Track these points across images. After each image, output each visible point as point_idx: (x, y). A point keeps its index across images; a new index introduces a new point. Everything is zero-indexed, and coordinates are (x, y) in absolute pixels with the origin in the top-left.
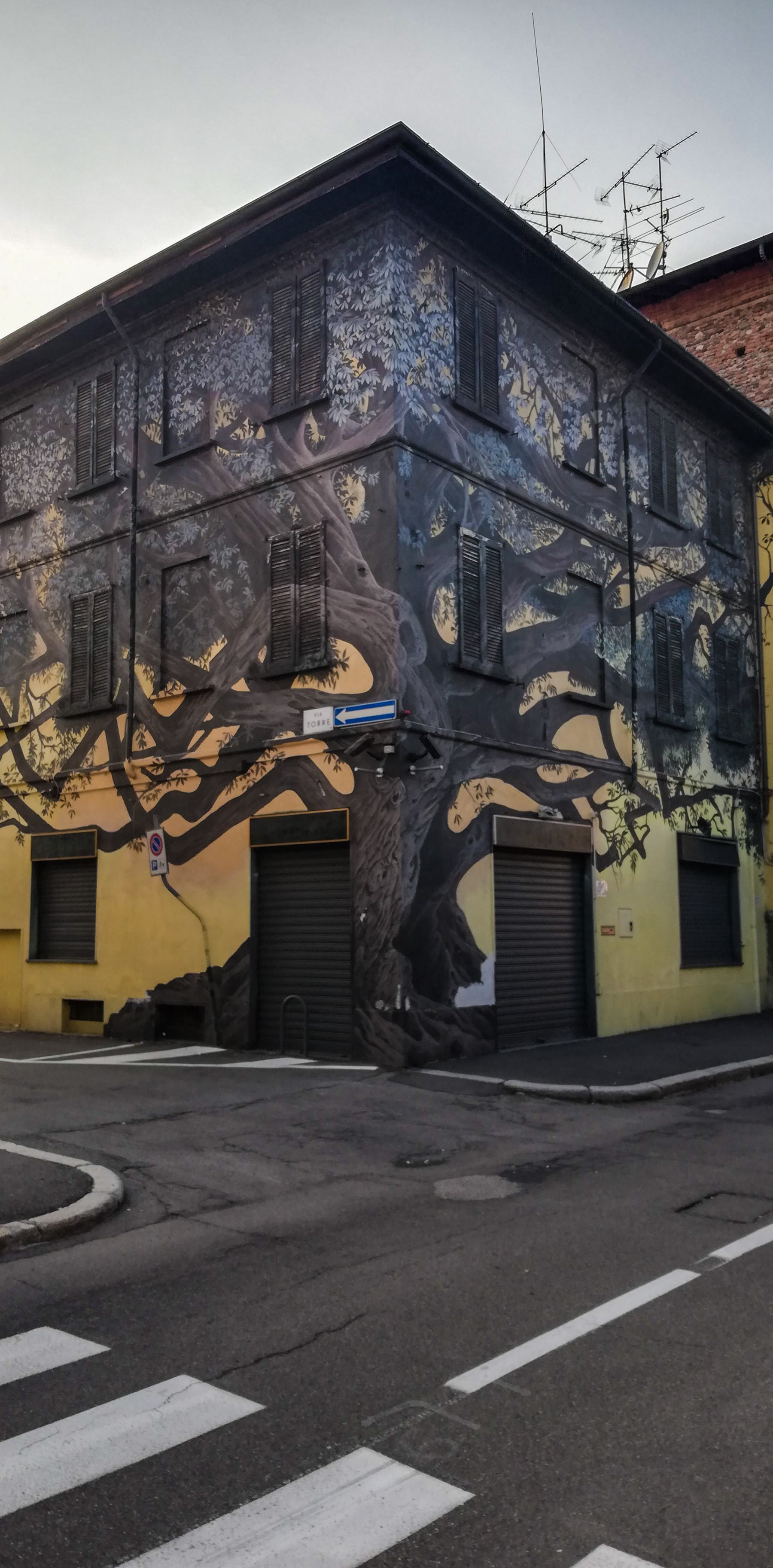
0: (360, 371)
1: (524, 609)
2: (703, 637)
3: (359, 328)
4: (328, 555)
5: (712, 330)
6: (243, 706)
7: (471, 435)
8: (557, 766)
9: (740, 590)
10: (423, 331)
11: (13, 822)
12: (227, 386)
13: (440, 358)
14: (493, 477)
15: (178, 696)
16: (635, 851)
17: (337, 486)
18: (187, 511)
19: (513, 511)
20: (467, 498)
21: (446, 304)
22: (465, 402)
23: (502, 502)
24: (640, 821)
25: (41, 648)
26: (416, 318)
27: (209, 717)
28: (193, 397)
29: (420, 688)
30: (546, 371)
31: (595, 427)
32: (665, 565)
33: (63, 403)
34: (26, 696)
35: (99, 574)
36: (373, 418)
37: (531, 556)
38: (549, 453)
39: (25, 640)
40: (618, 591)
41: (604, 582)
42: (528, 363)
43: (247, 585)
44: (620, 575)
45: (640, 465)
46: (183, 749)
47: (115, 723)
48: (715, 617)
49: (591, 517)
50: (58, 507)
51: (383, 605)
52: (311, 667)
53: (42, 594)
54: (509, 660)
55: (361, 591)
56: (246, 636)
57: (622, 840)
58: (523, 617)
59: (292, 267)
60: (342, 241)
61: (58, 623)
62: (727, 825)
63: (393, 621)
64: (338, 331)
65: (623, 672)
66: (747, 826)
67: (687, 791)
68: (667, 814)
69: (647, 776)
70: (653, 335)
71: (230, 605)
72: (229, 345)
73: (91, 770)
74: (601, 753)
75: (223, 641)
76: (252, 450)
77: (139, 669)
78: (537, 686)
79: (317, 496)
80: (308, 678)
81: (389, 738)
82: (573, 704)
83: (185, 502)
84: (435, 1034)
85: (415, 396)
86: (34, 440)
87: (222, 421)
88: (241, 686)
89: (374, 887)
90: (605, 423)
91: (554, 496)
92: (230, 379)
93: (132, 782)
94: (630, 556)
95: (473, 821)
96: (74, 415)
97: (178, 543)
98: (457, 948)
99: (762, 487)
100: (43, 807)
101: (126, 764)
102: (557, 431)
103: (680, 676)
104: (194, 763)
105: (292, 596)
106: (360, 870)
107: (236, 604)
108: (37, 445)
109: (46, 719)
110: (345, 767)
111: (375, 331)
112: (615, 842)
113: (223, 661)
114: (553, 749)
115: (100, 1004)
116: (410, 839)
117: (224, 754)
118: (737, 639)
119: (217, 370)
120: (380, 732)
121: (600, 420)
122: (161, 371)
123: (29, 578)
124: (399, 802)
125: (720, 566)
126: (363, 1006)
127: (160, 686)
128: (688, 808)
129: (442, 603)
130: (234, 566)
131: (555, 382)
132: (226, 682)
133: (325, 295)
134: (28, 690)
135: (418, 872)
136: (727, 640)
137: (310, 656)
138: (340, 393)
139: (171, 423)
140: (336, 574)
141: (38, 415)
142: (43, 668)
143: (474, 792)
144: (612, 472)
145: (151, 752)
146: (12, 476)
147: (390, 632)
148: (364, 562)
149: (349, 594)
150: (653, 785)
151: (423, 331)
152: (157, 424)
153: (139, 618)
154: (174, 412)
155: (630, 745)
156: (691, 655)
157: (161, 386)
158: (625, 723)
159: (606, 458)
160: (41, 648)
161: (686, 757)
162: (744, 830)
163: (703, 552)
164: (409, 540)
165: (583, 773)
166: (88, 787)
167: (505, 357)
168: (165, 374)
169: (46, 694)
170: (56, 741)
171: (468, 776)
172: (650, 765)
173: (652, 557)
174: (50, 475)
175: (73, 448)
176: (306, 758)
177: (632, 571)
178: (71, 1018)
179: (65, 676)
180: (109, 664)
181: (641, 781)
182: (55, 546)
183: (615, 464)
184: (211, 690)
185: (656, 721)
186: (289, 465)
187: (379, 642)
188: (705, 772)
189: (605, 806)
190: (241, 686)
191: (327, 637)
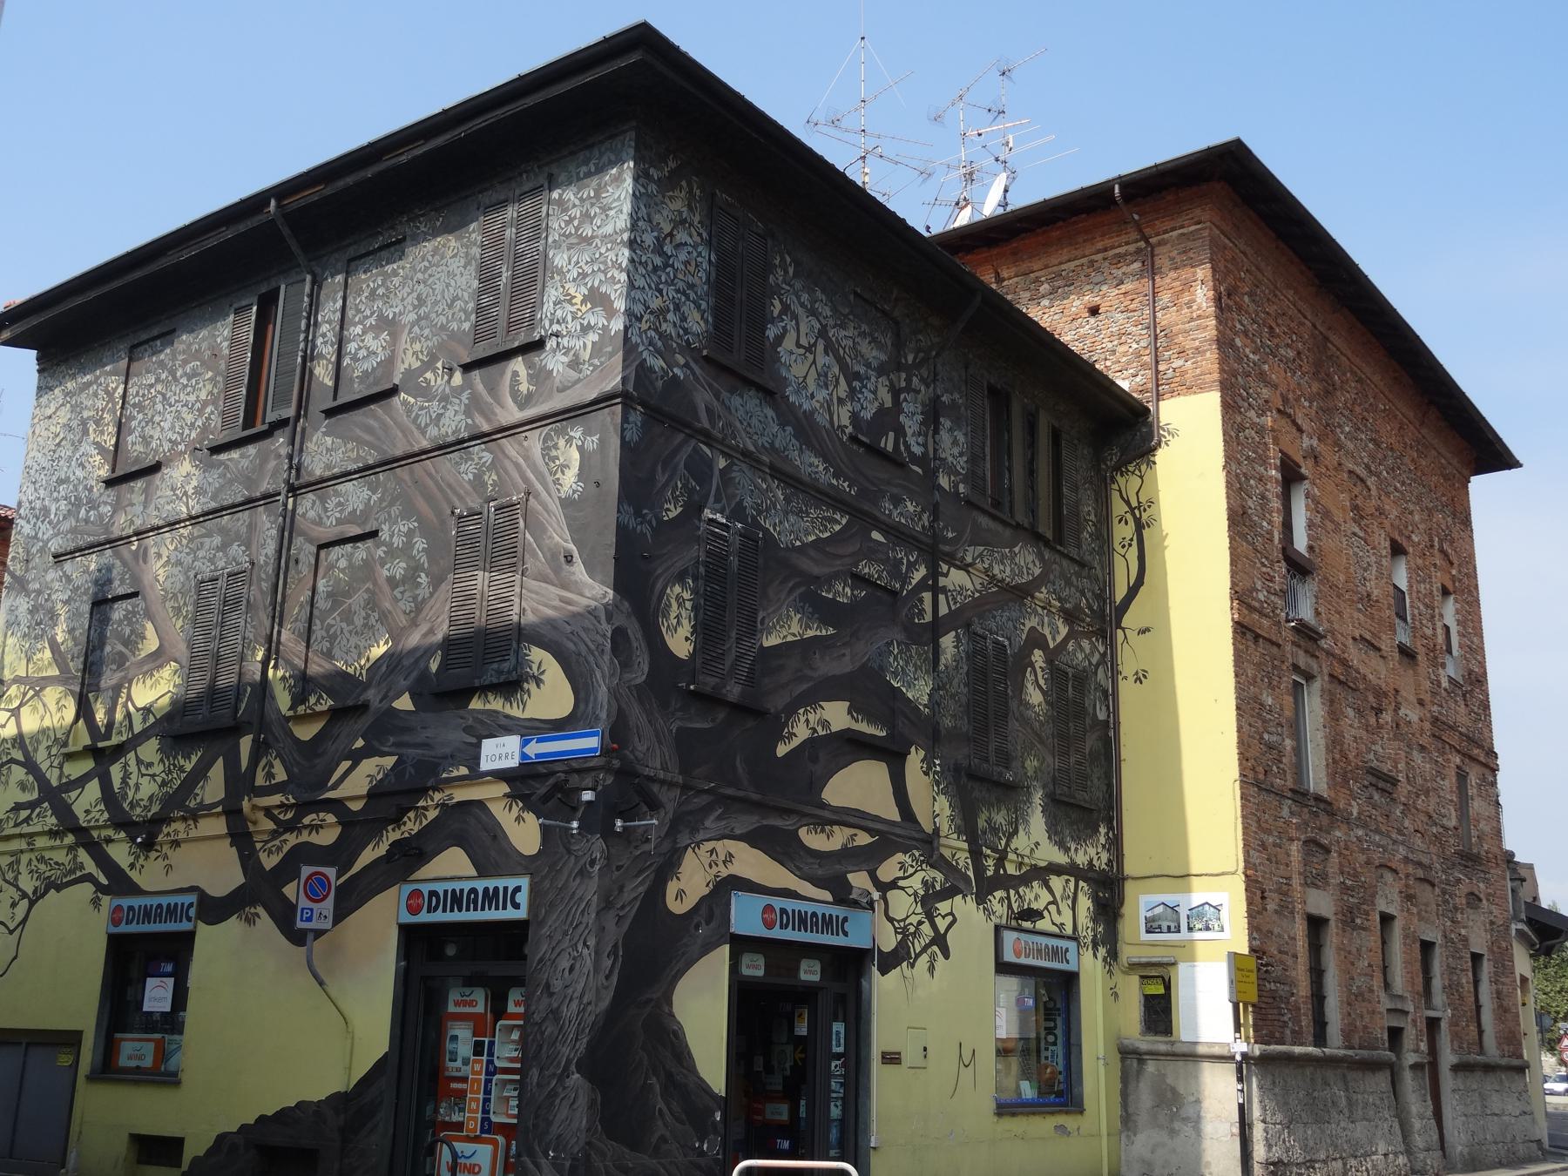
0: (584, 309)
1: (789, 617)
2: (1037, 666)
5: (1060, 283)
8: (827, 828)
9: (1090, 607)
10: (666, 265)
11: (89, 878)
12: (420, 318)
13: (688, 298)
14: (752, 448)
15: (322, 713)
16: (935, 948)
17: (546, 450)
18: (356, 472)
20: (717, 473)
21: (700, 235)
24: (944, 907)
25: (151, 643)
26: (659, 249)
27: (360, 743)
28: (377, 329)
29: (636, 714)
30: (831, 322)
31: (895, 392)
32: (986, 570)
35: (236, 550)
40: (921, 600)
41: (902, 587)
42: (808, 310)
43: (423, 570)
44: (924, 579)
45: (955, 443)
46: (322, 785)
48: (1054, 639)
49: (887, 505)
50: (193, 458)
52: (495, 681)
58: (787, 628)
61: (177, 611)
62: (1066, 917)
64: (560, 259)
65: (925, 706)
66: (1095, 920)
67: (1011, 869)
68: (981, 899)
69: (955, 847)
71: (399, 596)
72: (426, 268)
73: (199, 809)
74: (894, 814)
75: (386, 643)
76: (445, 399)
78: (803, 719)
79: (521, 461)
80: (491, 697)
81: (589, 781)
82: (852, 747)
83: (355, 461)
86: (172, 373)
87: (409, 360)
88: (404, 703)
89: (557, 985)
90: (908, 389)
91: (836, 476)
93: (252, 828)
94: (935, 554)
95: (703, 899)
96: (226, 344)
97: (341, 512)
98: (669, 1075)
99: (1118, 477)
100: (131, 859)
102: (843, 395)
103: (1004, 716)
104: (336, 806)
106: (541, 960)
107: (407, 594)
108: (175, 379)
109: (149, 738)
110: (530, 817)
111: (605, 263)
112: (906, 935)
113: (384, 668)
114: (824, 806)
115: (179, 1142)
116: (610, 921)
117: (374, 795)
118: (1084, 670)
120: (578, 771)
123: (146, 550)
124: (597, 867)
125: (1063, 575)
126: (532, 1155)
128: (1012, 892)
129: (675, 605)
130: (409, 545)
131: (843, 336)
134: (129, 698)
136: (1070, 670)
137: (495, 666)
139: (346, 361)
140: (537, 561)
143: (706, 859)
146: (140, 416)
147: (600, 640)
148: (572, 546)
150: (963, 859)
151: (666, 265)
152: (329, 361)
154: (351, 347)
155: (934, 807)
156: (1021, 687)
157: (338, 315)
158: (926, 773)
159: (909, 432)
160: (151, 643)
162: (1091, 925)
165: (864, 839)
166: (193, 833)
167: (777, 303)
171: (700, 837)
172: (959, 832)
173: (969, 559)
174: (189, 418)
176: (480, 804)
178: (139, 1162)
179: (178, 681)
182: (184, 509)
183: (920, 440)
184: (364, 708)
186: (489, 420)
187: (584, 650)
188: (1037, 844)
189: (894, 885)
190: (404, 703)
191: (519, 643)
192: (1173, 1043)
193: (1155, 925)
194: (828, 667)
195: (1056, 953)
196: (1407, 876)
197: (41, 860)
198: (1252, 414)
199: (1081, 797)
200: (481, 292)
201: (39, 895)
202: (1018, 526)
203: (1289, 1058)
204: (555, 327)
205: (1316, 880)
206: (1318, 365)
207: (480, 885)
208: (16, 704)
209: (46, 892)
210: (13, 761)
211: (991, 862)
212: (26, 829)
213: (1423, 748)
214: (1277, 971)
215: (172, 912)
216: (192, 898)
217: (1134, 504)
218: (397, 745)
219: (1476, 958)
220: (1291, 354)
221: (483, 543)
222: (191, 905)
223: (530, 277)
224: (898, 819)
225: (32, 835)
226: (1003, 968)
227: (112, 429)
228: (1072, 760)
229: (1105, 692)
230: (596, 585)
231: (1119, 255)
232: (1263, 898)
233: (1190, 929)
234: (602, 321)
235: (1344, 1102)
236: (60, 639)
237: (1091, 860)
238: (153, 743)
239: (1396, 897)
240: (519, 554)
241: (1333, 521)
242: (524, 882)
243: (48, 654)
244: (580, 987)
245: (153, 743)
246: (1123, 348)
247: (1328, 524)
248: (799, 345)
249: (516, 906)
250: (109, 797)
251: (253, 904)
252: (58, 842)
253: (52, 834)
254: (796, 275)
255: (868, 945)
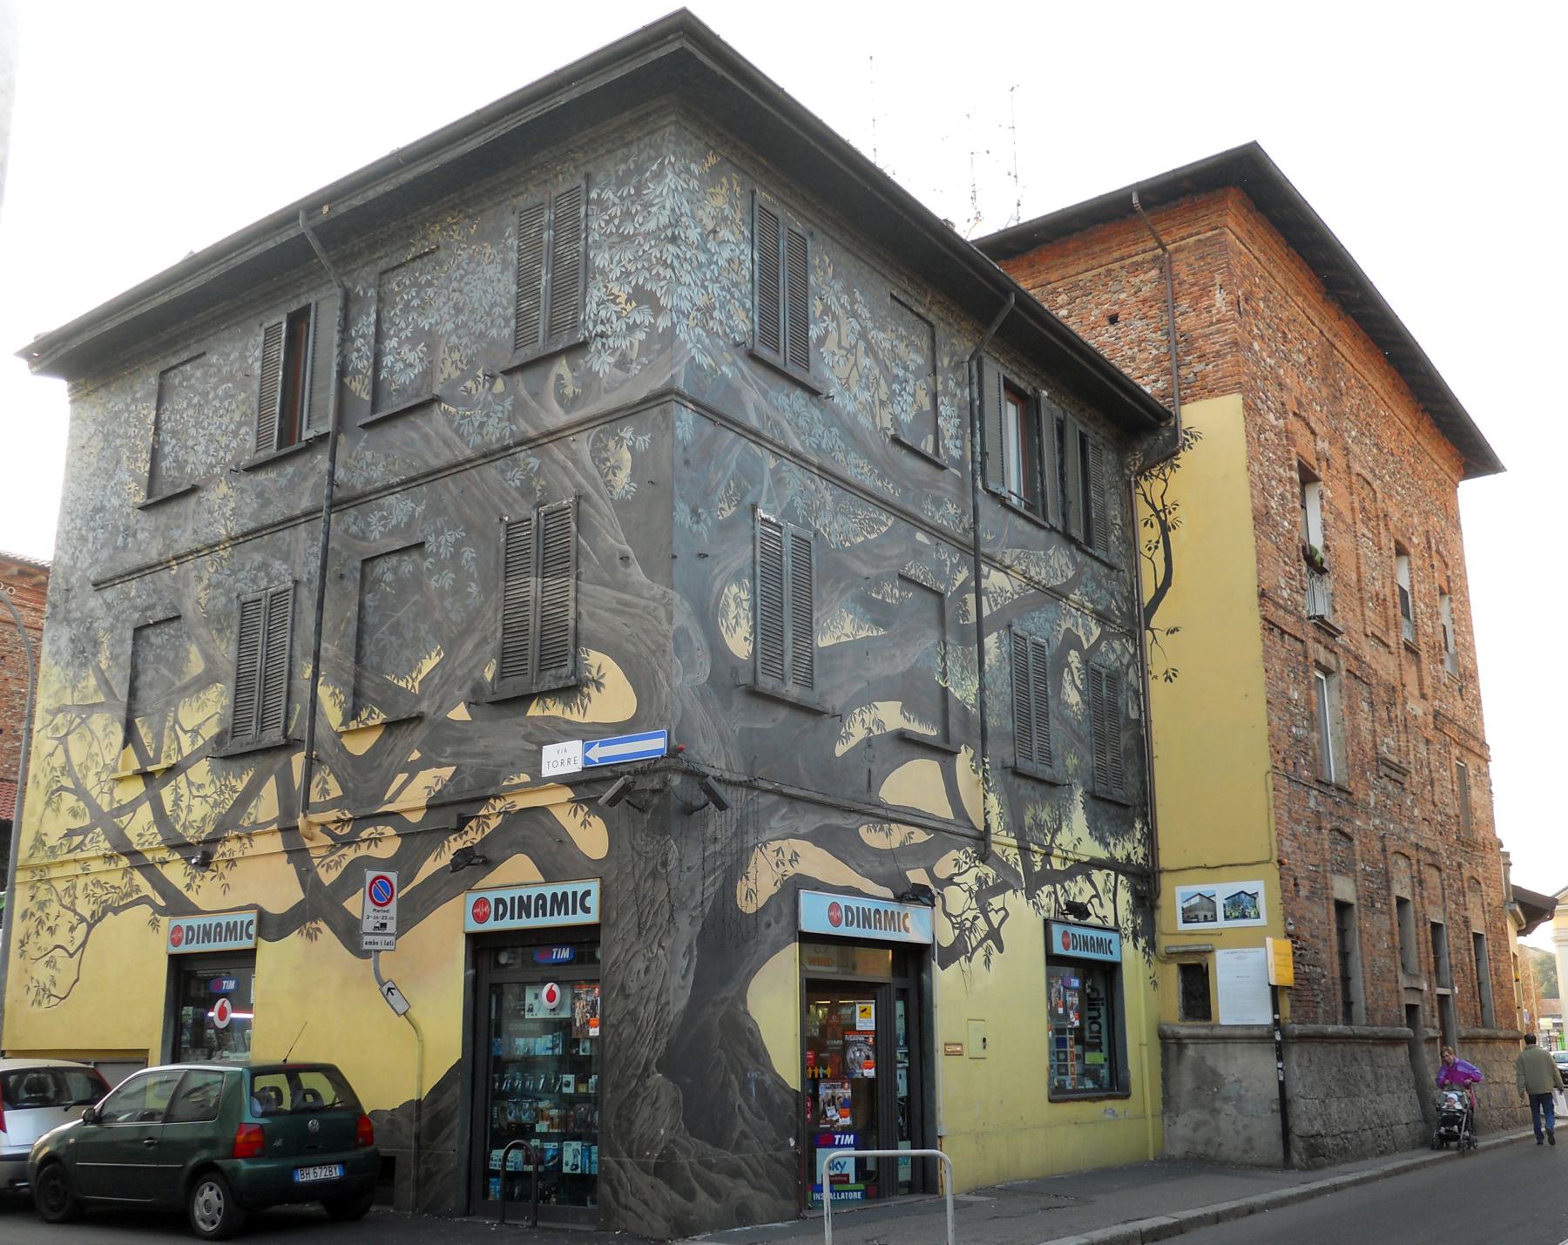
0: (629, 308)
3: (629, 255)
4: (582, 540)
6: (460, 741)
7: (772, 394)
9: (1119, 609)
10: (710, 263)
11: (145, 900)
12: (457, 327)
14: (800, 449)
15: (374, 727)
16: (990, 942)
17: (595, 452)
18: (398, 485)
19: (827, 495)
20: (767, 472)
22: (765, 353)
23: (813, 481)
24: (996, 902)
25: (196, 665)
27: (416, 755)
28: (413, 341)
33: (245, 348)
34: (173, 728)
36: (643, 366)
37: (853, 550)
38: (874, 423)
39: (177, 656)
40: (965, 602)
46: (378, 799)
47: (289, 763)
51: (653, 604)
53: (202, 594)
54: (821, 683)
55: (623, 587)
56: (469, 646)
57: (972, 928)
58: (839, 628)
59: (546, 181)
60: (609, 152)
62: (1108, 911)
63: (665, 626)
64: (601, 259)
66: (1134, 913)
67: (1057, 864)
68: (1030, 894)
69: (1004, 843)
70: (1007, 287)
71: (449, 607)
72: (462, 277)
74: (948, 813)
75: (438, 654)
77: (323, 692)
78: (859, 719)
82: (907, 743)
84: (715, 1193)
85: (699, 341)
86: (205, 394)
87: (449, 371)
88: (460, 713)
89: (633, 987)
91: (881, 477)
92: (462, 318)
93: (308, 844)
94: (975, 554)
96: (258, 365)
97: (384, 526)
99: (1143, 482)
101: (300, 821)
103: (1044, 716)
105: (532, 593)
106: (614, 963)
111: (649, 260)
112: (962, 929)
113: (437, 680)
119: (446, 309)
120: (643, 773)
121: (940, 388)
122: (373, 308)
125: (1094, 577)
127: (352, 713)
130: (456, 556)
131: (880, 337)
132: (439, 708)
133: (587, 215)
134: (176, 721)
135: (694, 965)
138: (602, 335)
139: (383, 375)
141: (211, 366)
142: (198, 691)
143: (773, 858)
144: (956, 453)
145: (336, 803)
149: (607, 591)
150: (1012, 855)
151: (710, 263)
153: (327, 626)
154: (388, 360)
156: (1059, 687)
157: (372, 329)
158: (975, 772)
159: (947, 435)
160: (196, 665)
161: (1054, 820)
163: (1073, 558)
164: (688, 521)
165: (920, 836)
166: (249, 852)
167: (818, 303)
168: (378, 313)
169: (199, 726)
170: (209, 790)
171: (765, 837)
172: (1008, 828)
175: (255, 405)
177: (978, 576)
180: (285, 686)
181: (996, 848)
182: (223, 532)
183: (958, 443)
185: (1016, 773)
187: (645, 652)
189: (950, 881)
190: (460, 713)
191: (576, 647)
192: (1212, 1027)
193: (1192, 915)
194: (879, 669)
195: (1101, 945)
196: (1418, 861)
197: (97, 884)
198: (1271, 417)
199: (1117, 794)
200: (519, 297)
201: (96, 919)
202: (1052, 529)
203: (1323, 1038)
204: (600, 328)
205: (1345, 868)
206: (1326, 370)
207: (548, 891)
208: (63, 733)
209: (104, 914)
210: (62, 788)
211: (1038, 858)
212: (79, 855)
213: (1428, 741)
214: (1309, 955)
215: (232, 930)
216: (252, 916)
217: (1159, 507)
218: (456, 755)
219: (1477, 937)
220: (1302, 359)
221: (534, 550)
222: (250, 923)
223: (572, 278)
224: (951, 817)
225: (86, 860)
226: (1053, 960)
227: (146, 456)
228: (1109, 758)
229: (1136, 692)
230: (655, 586)
231: (1136, 264)
232: (1296, 885)
233: (1226, 917)
234: (649, 319)
235: (1369, 1077)
236: (103, 666)
237: (1128, 856)
238: (204, 764)
239: (1407, 880)
240: (573, 558)
241: (1344, 522)
242: (594, 886)
243: (92, 682)
244: (657, 989)
245: (204, 764)
246: (1145, 355)
247: (1340, 524)
248: (840, 347)
249: (587, 910)
250: (160, 816)
251: (314, 919)
252: (113, 866)
253: (108, 858)
254: (834, 277)
255: (926, 940)
